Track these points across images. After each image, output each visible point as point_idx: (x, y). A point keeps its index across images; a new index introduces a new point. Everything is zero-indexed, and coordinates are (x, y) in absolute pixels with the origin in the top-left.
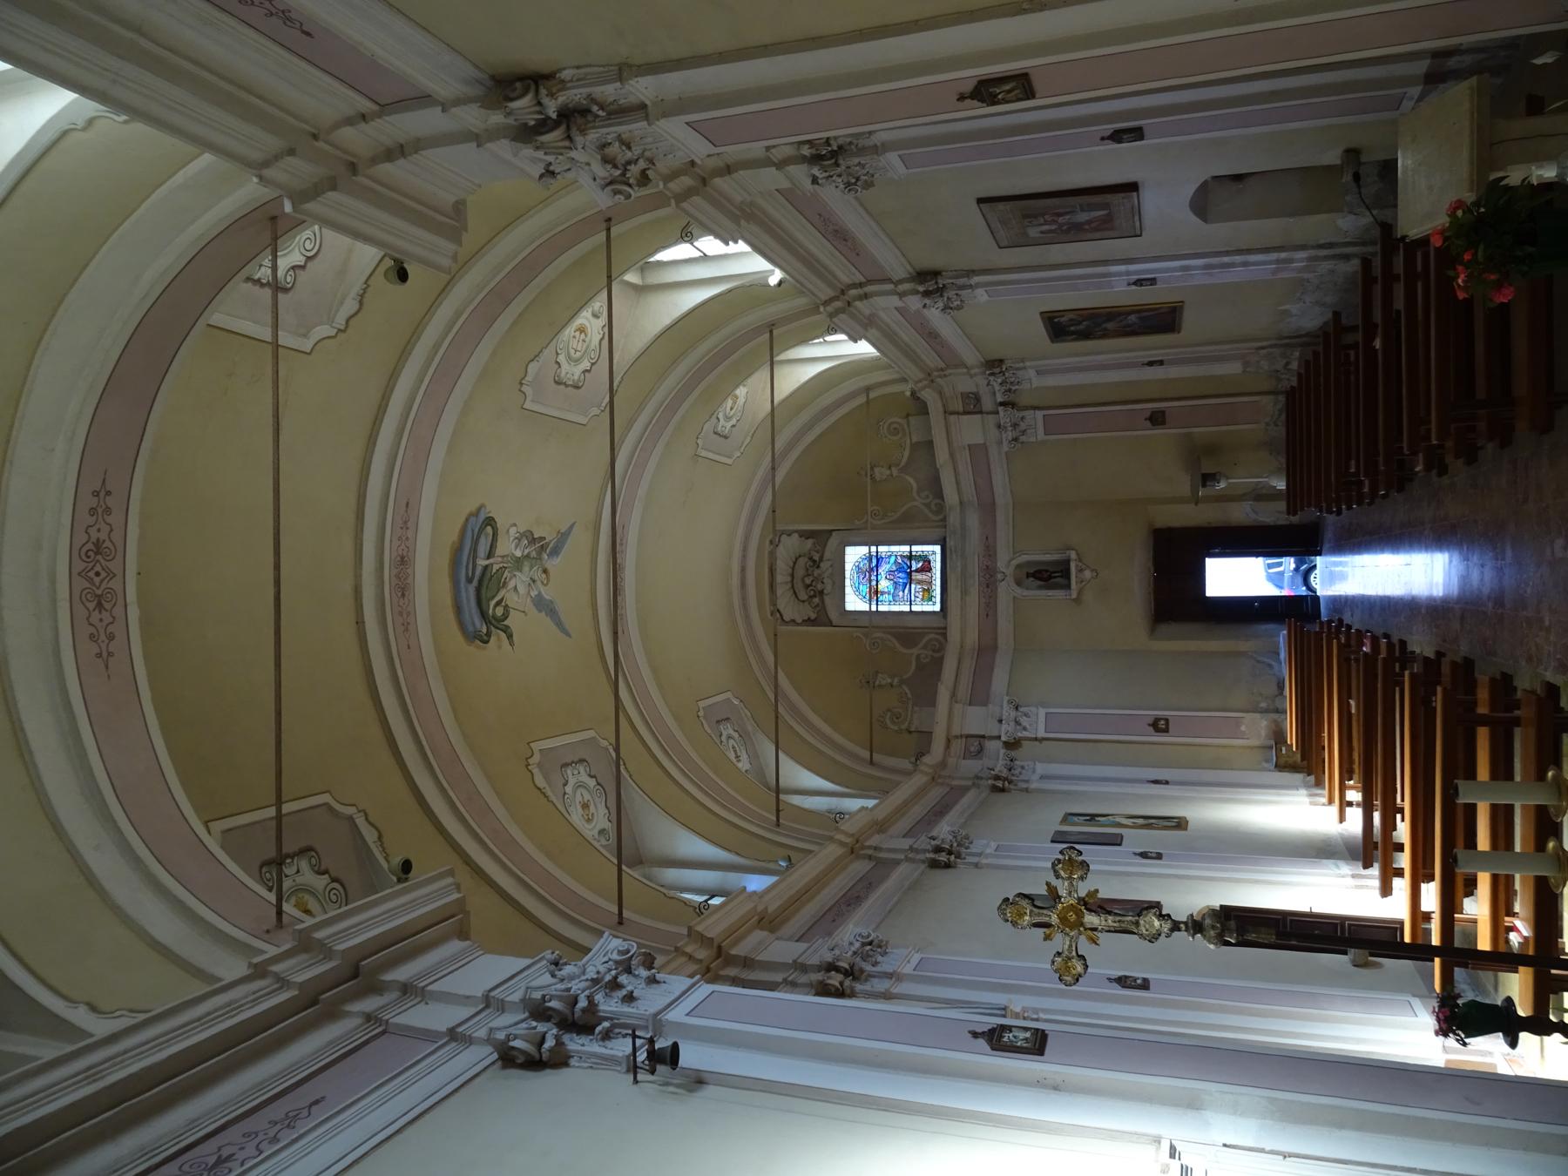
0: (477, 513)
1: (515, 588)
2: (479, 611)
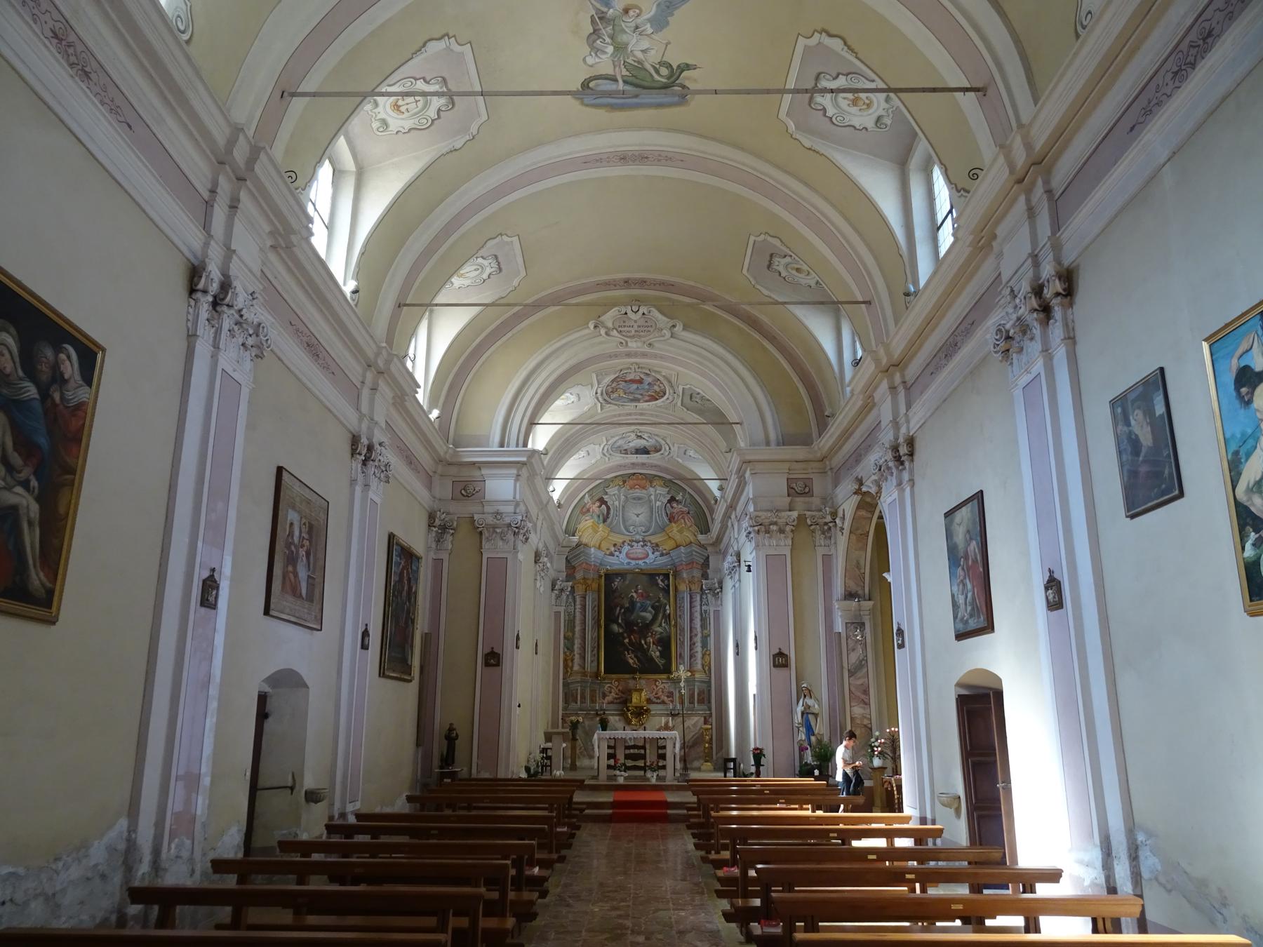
1: (644, 51)
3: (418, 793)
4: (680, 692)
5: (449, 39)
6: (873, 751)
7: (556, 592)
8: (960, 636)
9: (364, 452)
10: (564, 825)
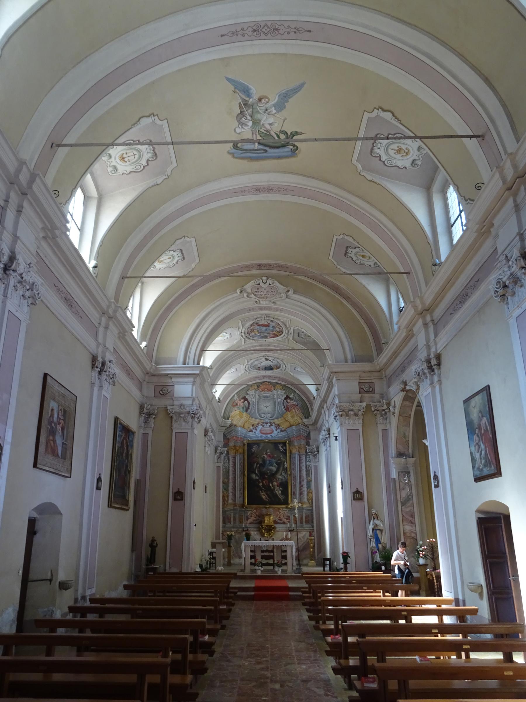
0: (232, 154)
1: (270, 124)
2: (281, 148)
3: (132, 583)
4: (294, 516)
5: (154, 116)
6: (419, 554)
7: (218, 454)
8: (477, 479)
9: (100, 366)
10: (224, 604)
